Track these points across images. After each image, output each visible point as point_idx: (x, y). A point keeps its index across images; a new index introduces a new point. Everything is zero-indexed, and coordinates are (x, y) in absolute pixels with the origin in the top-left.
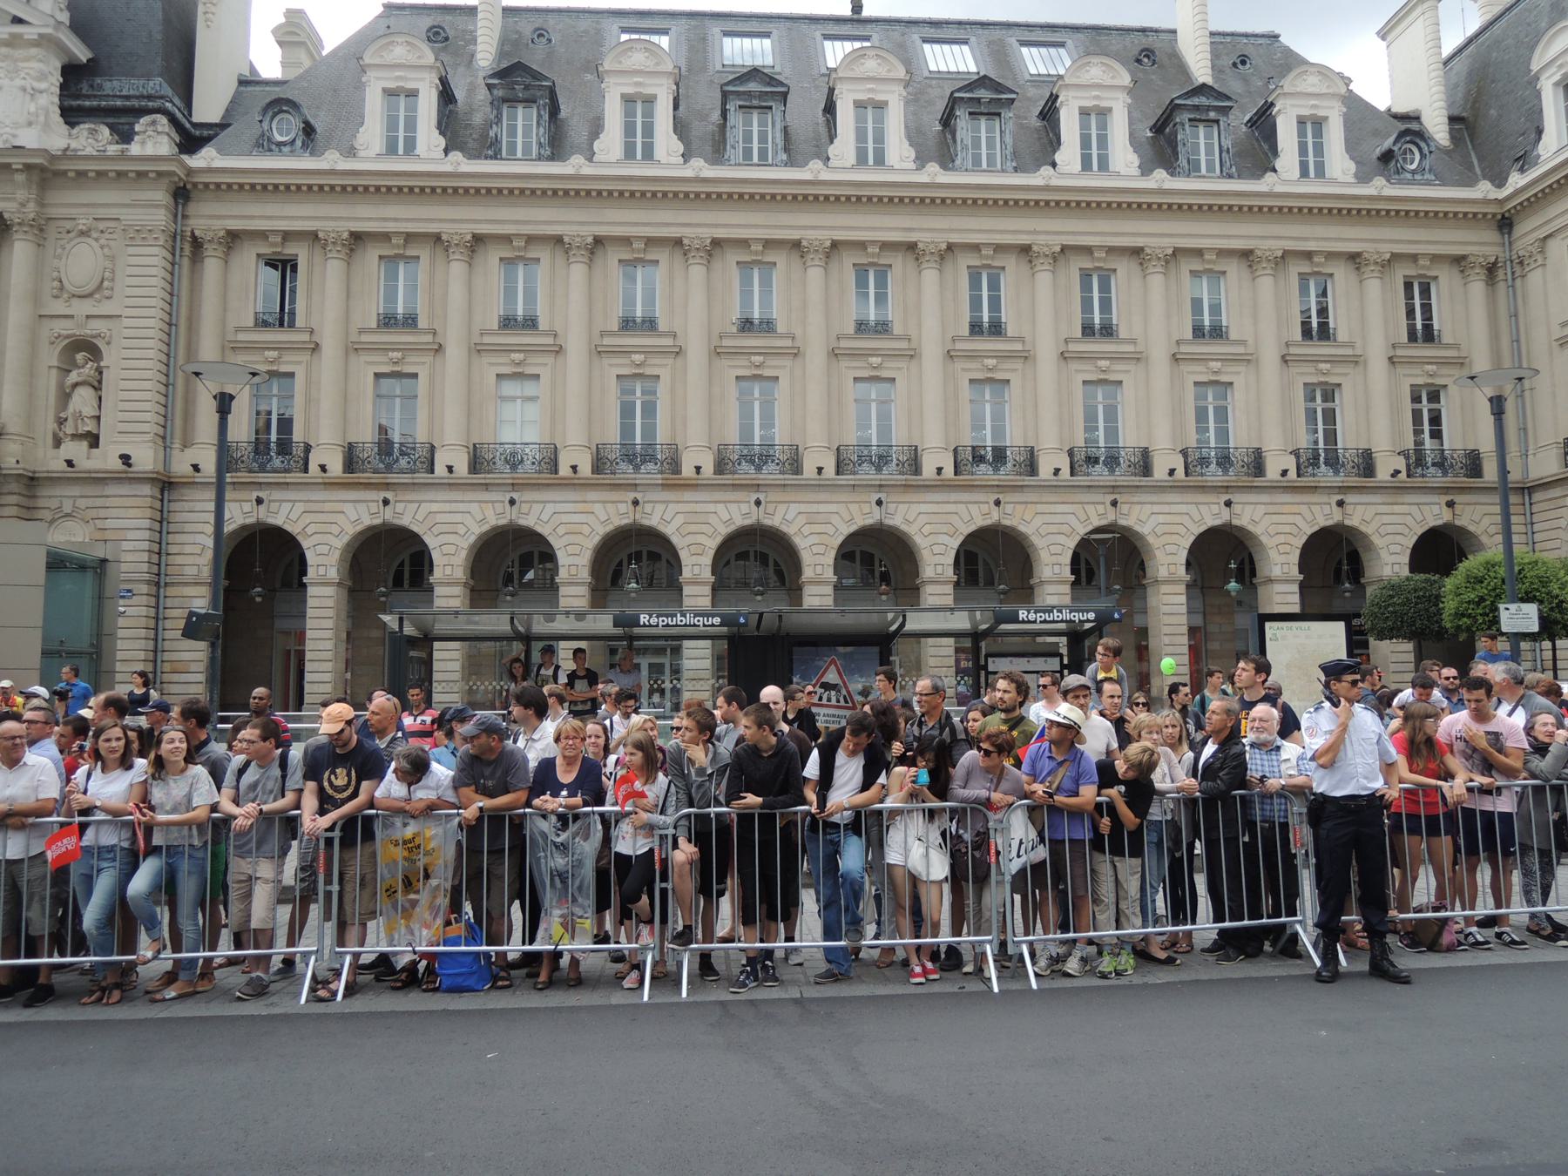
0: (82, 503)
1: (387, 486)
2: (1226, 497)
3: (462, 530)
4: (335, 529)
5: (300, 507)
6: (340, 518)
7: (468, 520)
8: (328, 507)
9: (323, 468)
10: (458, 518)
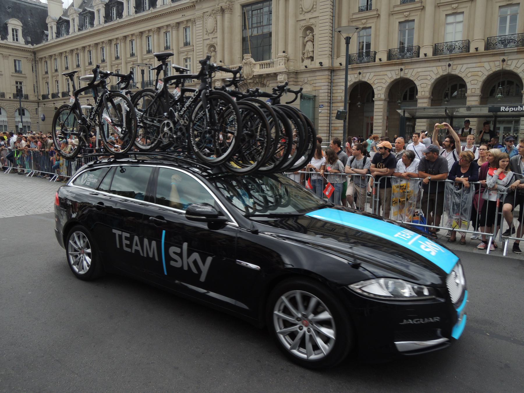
0: (309, 79)
1: (402, 64)
2: (358, 71)
3: (429, 78)
4: (384, 81)
5: (372, 74)
6: (385, 77)
7: (431, 74)
8: (381, 73)
9: (380, 60)
10: (428, 73)
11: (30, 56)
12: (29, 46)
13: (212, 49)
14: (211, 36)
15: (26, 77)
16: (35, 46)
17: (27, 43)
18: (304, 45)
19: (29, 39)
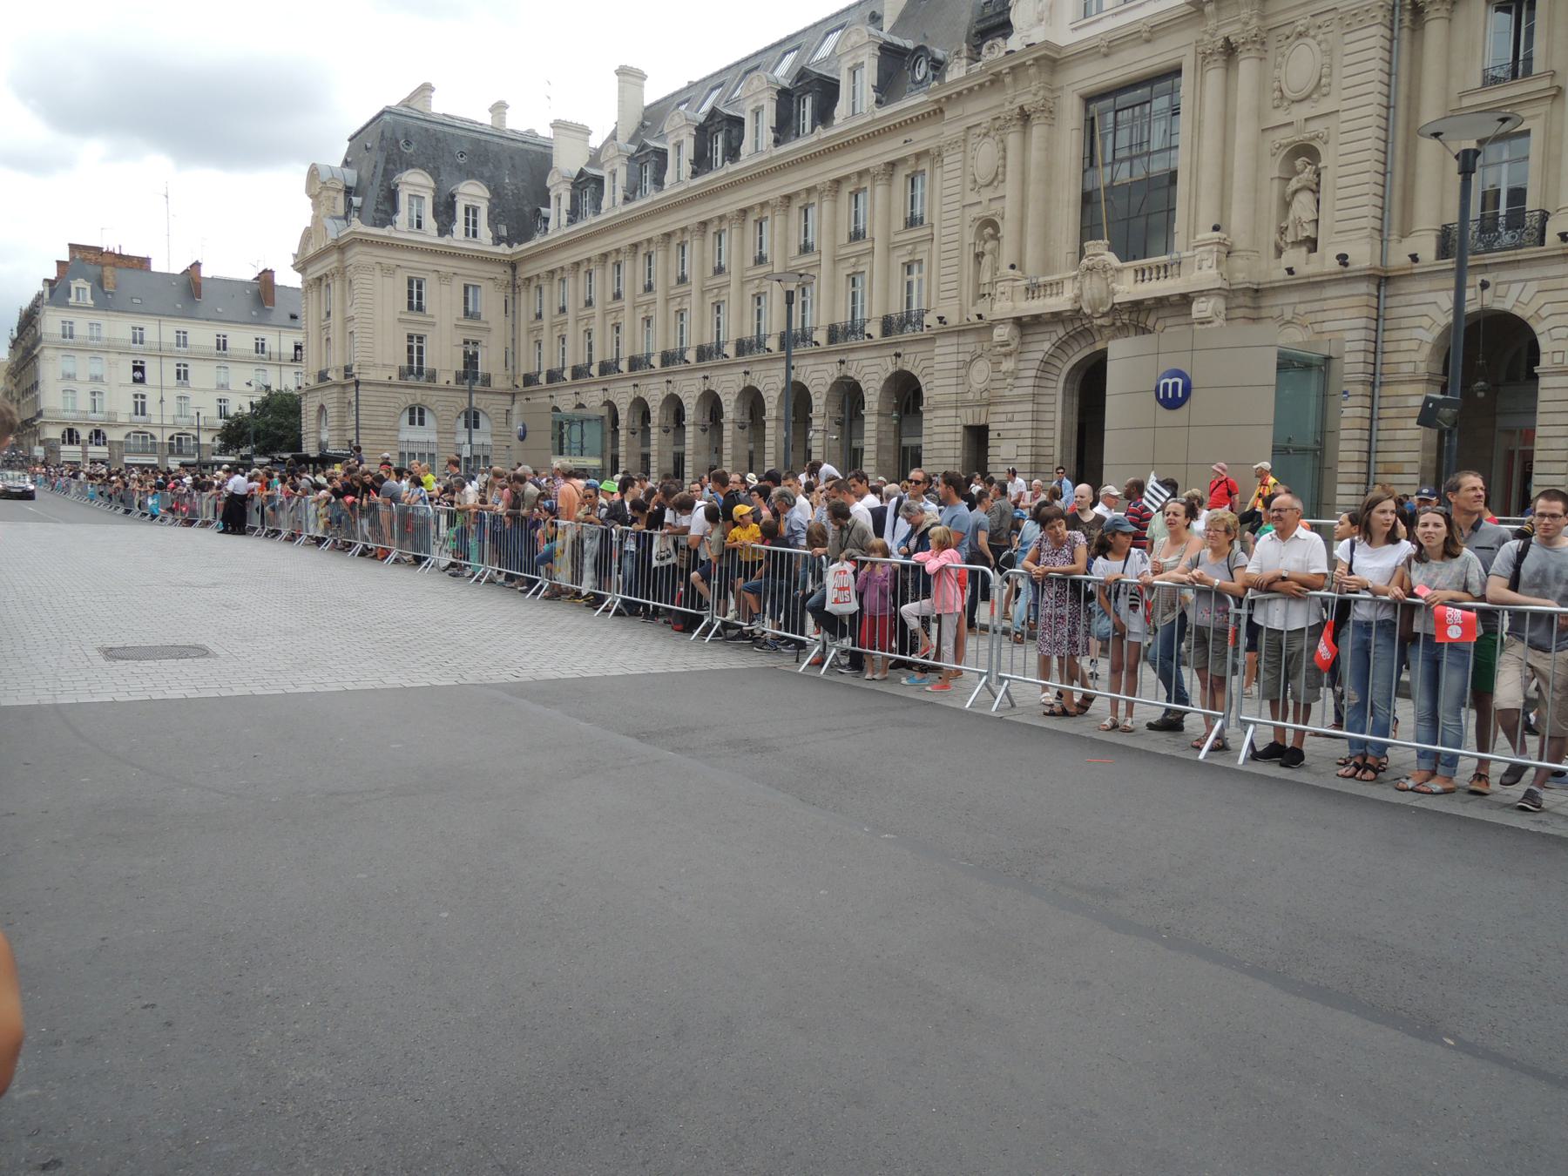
0: (1301, 309)
11: (501, 273)
12: (503, 248)
13: (989, 230)
14: (987, 194)
15: (489, 330)
16: (517, 248)
17: (498, 240)
18: (1286, 205)
19: (504, 232)
